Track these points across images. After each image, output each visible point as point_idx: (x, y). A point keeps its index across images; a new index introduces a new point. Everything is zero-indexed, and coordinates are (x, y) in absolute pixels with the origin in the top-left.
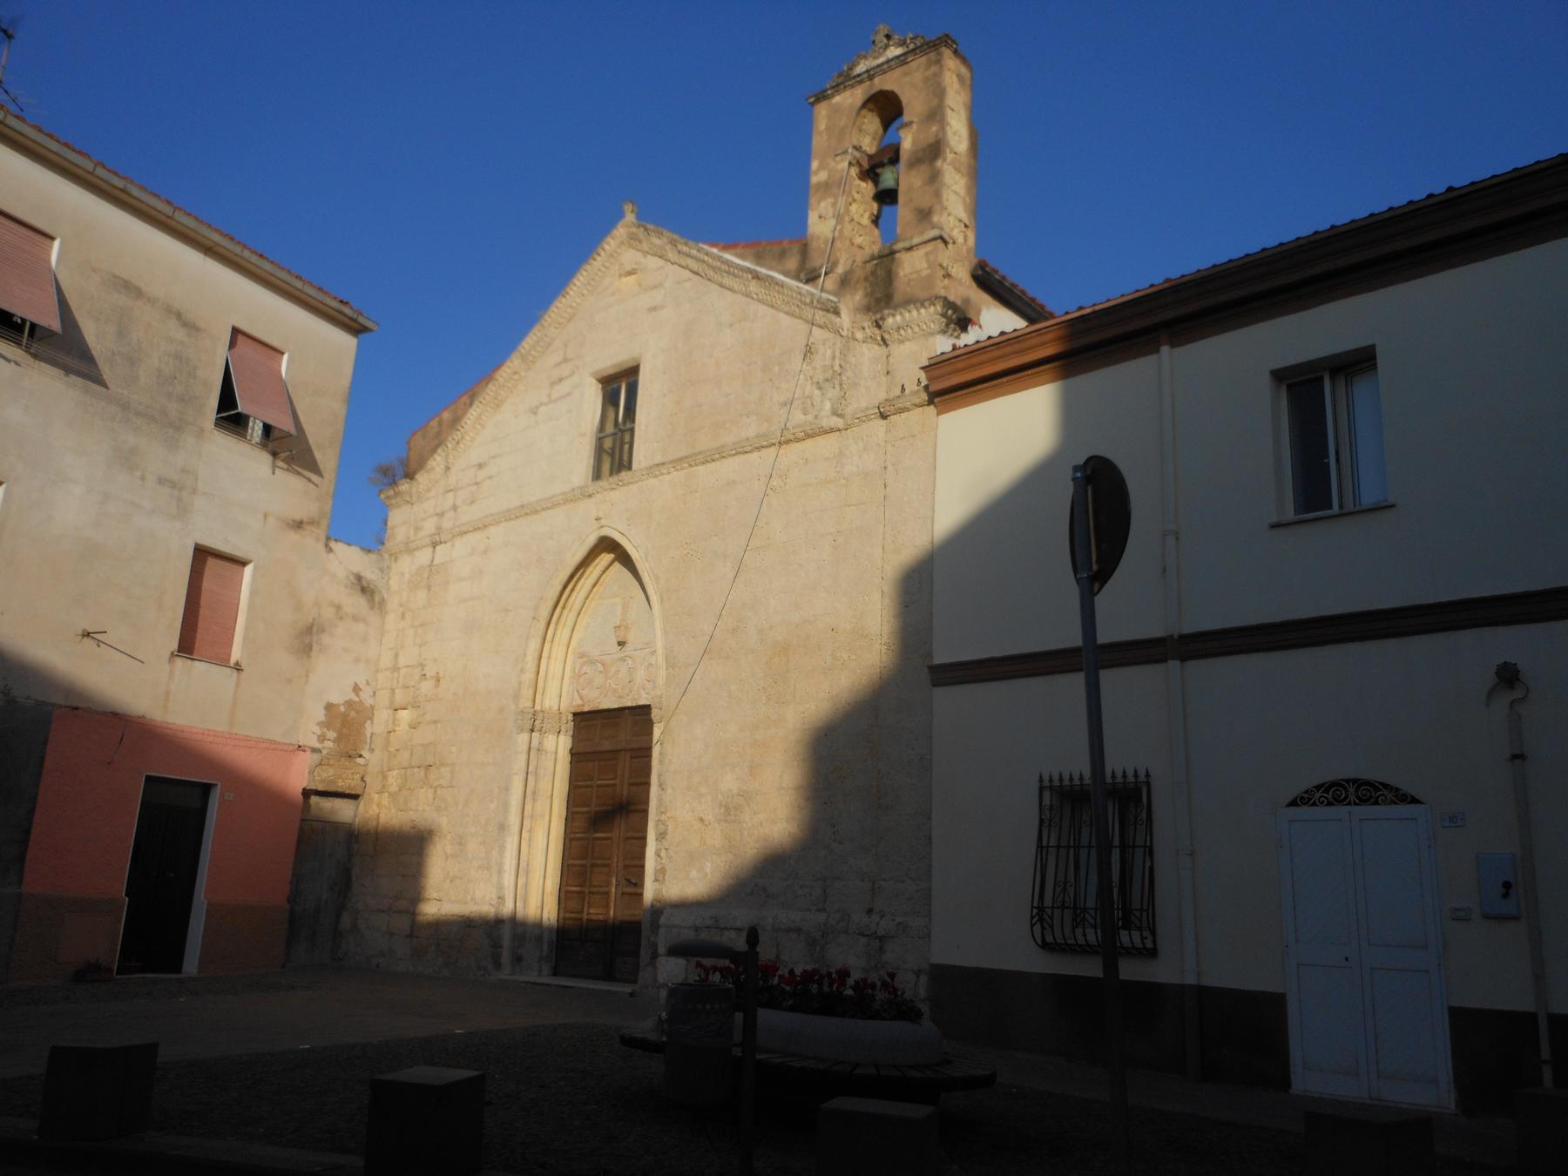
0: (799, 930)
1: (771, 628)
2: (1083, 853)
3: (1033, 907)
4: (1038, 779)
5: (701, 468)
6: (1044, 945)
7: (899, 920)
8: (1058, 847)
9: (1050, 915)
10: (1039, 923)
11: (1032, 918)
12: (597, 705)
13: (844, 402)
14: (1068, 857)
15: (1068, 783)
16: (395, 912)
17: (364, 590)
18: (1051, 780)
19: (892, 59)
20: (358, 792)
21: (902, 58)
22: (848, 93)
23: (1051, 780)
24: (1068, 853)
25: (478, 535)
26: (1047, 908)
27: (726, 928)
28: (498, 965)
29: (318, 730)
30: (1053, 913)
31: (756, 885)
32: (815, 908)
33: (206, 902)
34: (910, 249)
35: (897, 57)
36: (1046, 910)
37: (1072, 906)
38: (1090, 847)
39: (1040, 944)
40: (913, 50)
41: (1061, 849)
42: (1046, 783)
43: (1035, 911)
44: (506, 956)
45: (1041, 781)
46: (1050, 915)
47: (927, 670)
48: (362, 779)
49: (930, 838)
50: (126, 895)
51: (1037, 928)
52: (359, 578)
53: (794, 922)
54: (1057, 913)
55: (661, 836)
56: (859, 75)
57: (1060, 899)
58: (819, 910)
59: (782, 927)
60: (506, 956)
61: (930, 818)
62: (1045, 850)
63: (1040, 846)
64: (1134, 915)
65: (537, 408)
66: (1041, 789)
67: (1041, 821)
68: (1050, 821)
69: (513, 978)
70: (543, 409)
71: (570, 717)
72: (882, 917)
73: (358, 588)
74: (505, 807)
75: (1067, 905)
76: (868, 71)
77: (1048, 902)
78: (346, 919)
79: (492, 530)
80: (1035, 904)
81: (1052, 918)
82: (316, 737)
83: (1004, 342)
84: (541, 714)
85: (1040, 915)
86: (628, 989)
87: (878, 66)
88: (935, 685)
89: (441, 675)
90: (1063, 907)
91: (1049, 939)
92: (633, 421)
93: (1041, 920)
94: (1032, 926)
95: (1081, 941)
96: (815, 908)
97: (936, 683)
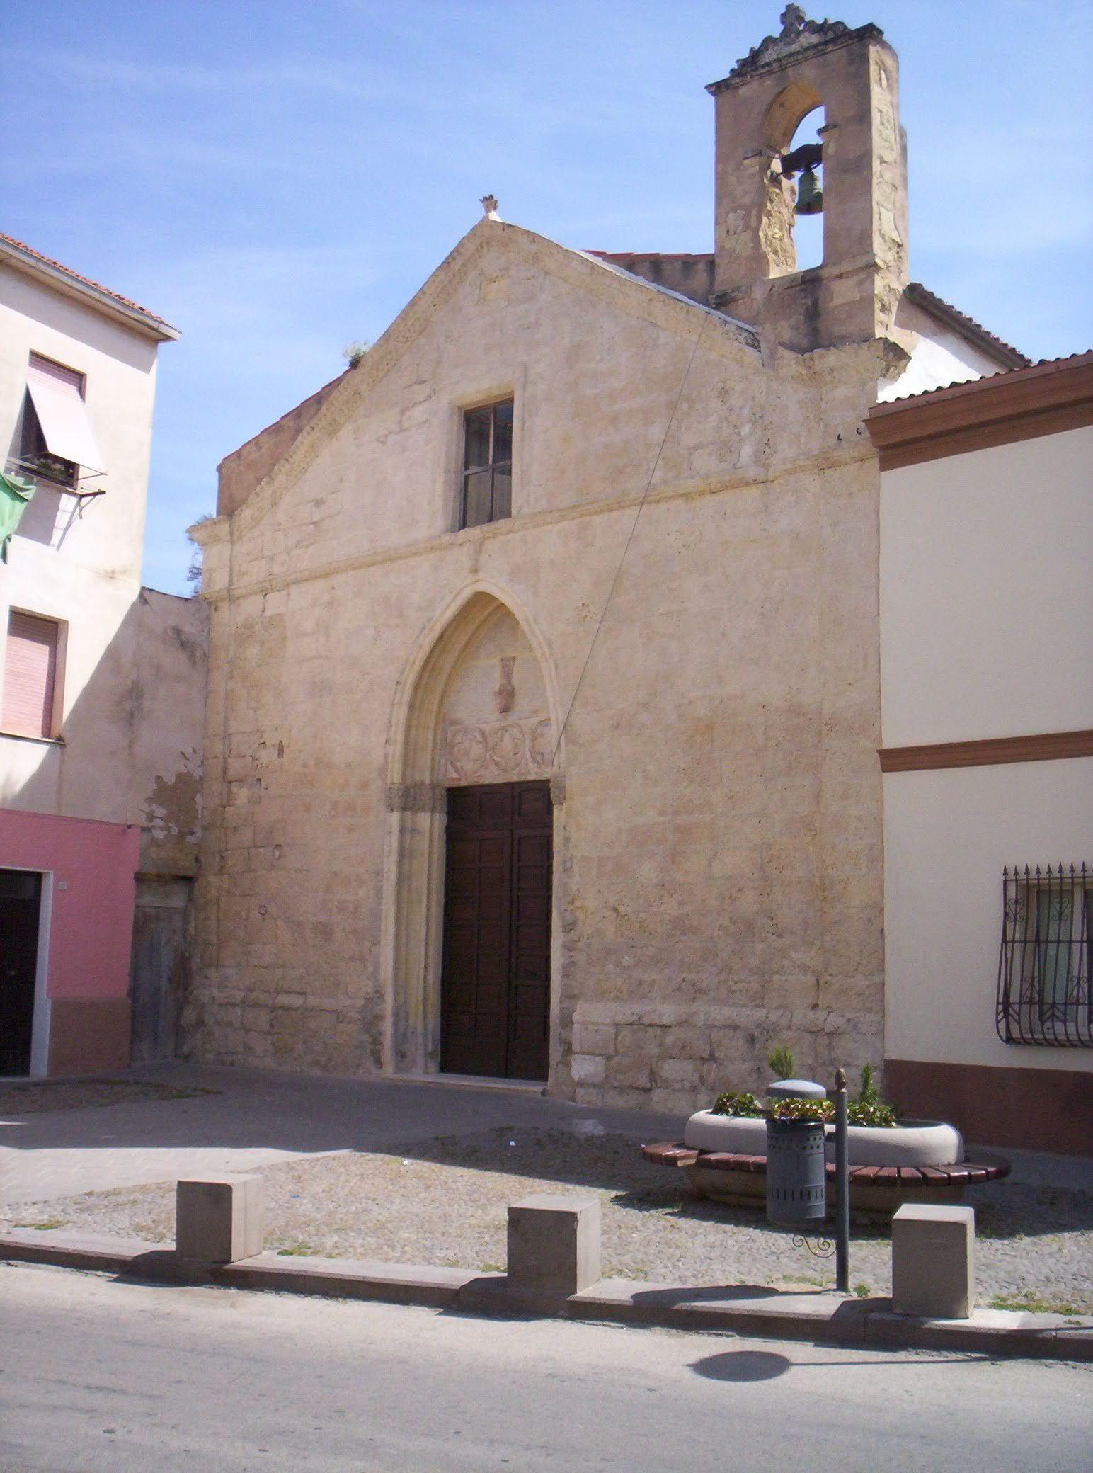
0: (736, 1028)
1: (690, 702)
2: (1076, 947)
3: (998, 1003)
4: (1003, 872)
5: (598, 519)
6: (1009, 1040)
7: (849, 1016)
8: (1025, 942)
9: (1017, 1011)
10: (1004, 1020)
11: (998, 1014)
12: (476, 779)
13: (768, 450)
14: (1081, 951)
15: (1058, 875)
16: (249, 1006)
17: (183, 645)
18: (1016, 873)
19: (807, 49)
20: (190, 873)
21: (820, 48)
22: (755, 84)
23: (1016, 873)
24: (1081, 947)
25: (320, 585)
26: (1015, 1004)
27: (650, 1025)
28: (378, 1062)
29: (145, 807)
30: (1020, 1008)
31: (684, 980)
32: (753, 1004)
33: (50, 1001)
34: (840, 276)
35: (815, 46)
36: (1058, 1006)
37: (1086, 1002)
38: (1082, 942)
39: (1004, 1038)
40: (832, 40)
41: (1028, 945)
42: (1011, 876)
43: (1001, 1007)
44: (388, 1054)
45: (1005, 873)
46: (1017, 1011)
47: (877, 755)
48: (197, 860)
49: (882, 931)
50: (47, 996)
51: (1002, 1024)
52: (178, 631)
53: (729, 1018)
54: (1025, 1008)
55: (568, 928)
56: (768, 64)
57: (1028, 994)
58: (757, 1006)
59: (716, 1023)
60: (388, 1054)
61: (882, 910)
62: (1010, 944)
63: (1004, 941)
64: (1058, 1009)
65: (386, 436)
66: (1005, 883)
67: (1006, 915)
68: (1016, 915)
69: (396, 1076)
70: (392, 438)
71: (444, 792)
72: (830, 1013)
73: (178, 644)
74: (379, 893)
75: (1081, 1001)
76: (779, 60)
77: (1015, 997)
78: (189, 1015)
79: (340, 579)
80: (1001, 1000)
81: (1019, 1014)
82: (144, 815)
83: (956, 394)
84: (412, 790)
85: (1005, 1006)
86: (534, 1088)
87: (791, 55)
88: (885, 771)
89: (285, 743)
90: (1031, 1003)
91: (1016, 1034)
92: (508, 456)
93: (1007, 1016)
94: (998, 1022)
95: (1050, 1037)
96: (753, 1004)
97: (887, 768)
